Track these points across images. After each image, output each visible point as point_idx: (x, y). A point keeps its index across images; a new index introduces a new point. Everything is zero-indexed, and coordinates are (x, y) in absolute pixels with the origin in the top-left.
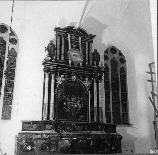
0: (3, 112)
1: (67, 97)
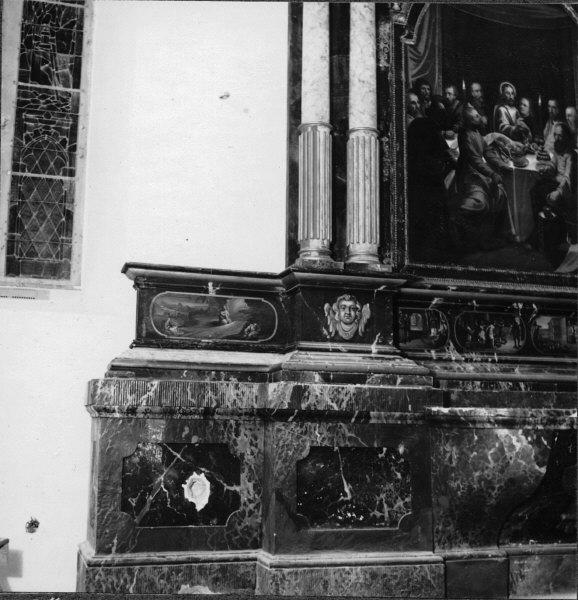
0: (14, 224)
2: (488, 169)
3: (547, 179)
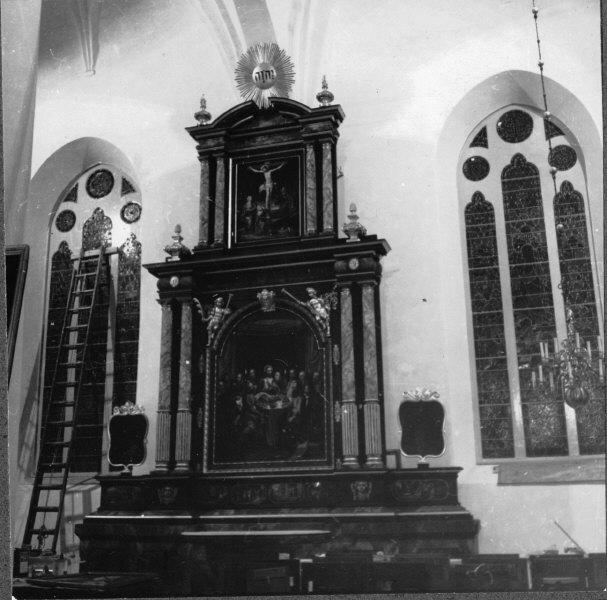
3: (287, 411)
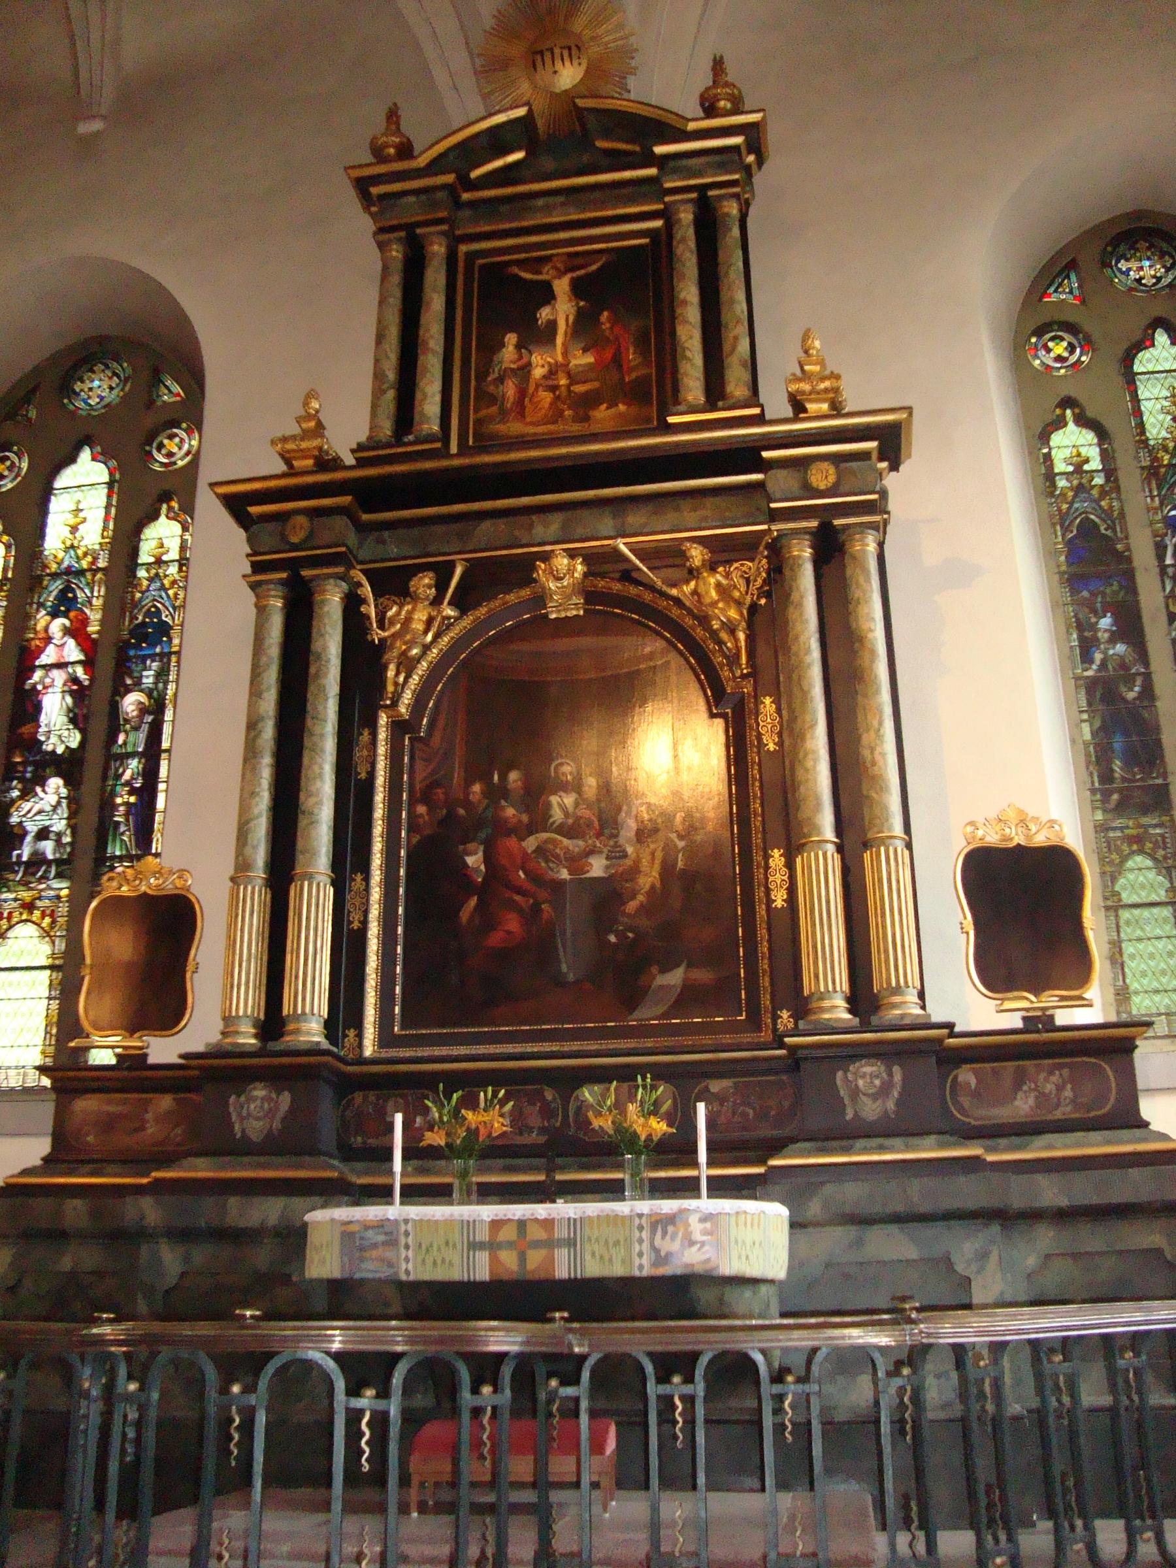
1: (498, 793)
2: (529, 886)
